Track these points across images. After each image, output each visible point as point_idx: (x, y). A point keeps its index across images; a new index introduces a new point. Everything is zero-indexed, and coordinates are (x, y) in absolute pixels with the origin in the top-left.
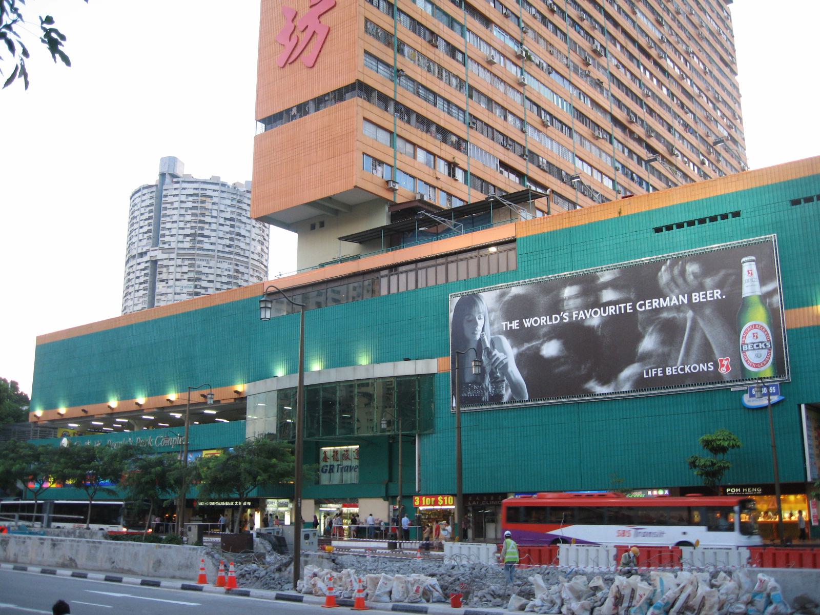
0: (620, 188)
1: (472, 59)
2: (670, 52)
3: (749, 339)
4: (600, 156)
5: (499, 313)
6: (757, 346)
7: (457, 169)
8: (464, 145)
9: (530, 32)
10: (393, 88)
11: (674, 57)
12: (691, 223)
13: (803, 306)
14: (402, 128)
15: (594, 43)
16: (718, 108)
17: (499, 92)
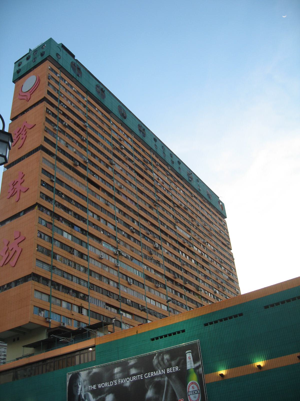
0: (171, 310)
1: (91, 258)
2: (195, 243)
3: (191, 389)
4: (160, 295)
5: (88, 382)
6: (194, 392)
7: (83, 309)
8: (87, 297)
9: (121, 243)
10: (50, 275)
11: (198, 246)
12: (166, 336)
13: (212, 372)
15: (155, 244)
16: (222, 266)
17: (105, 272)
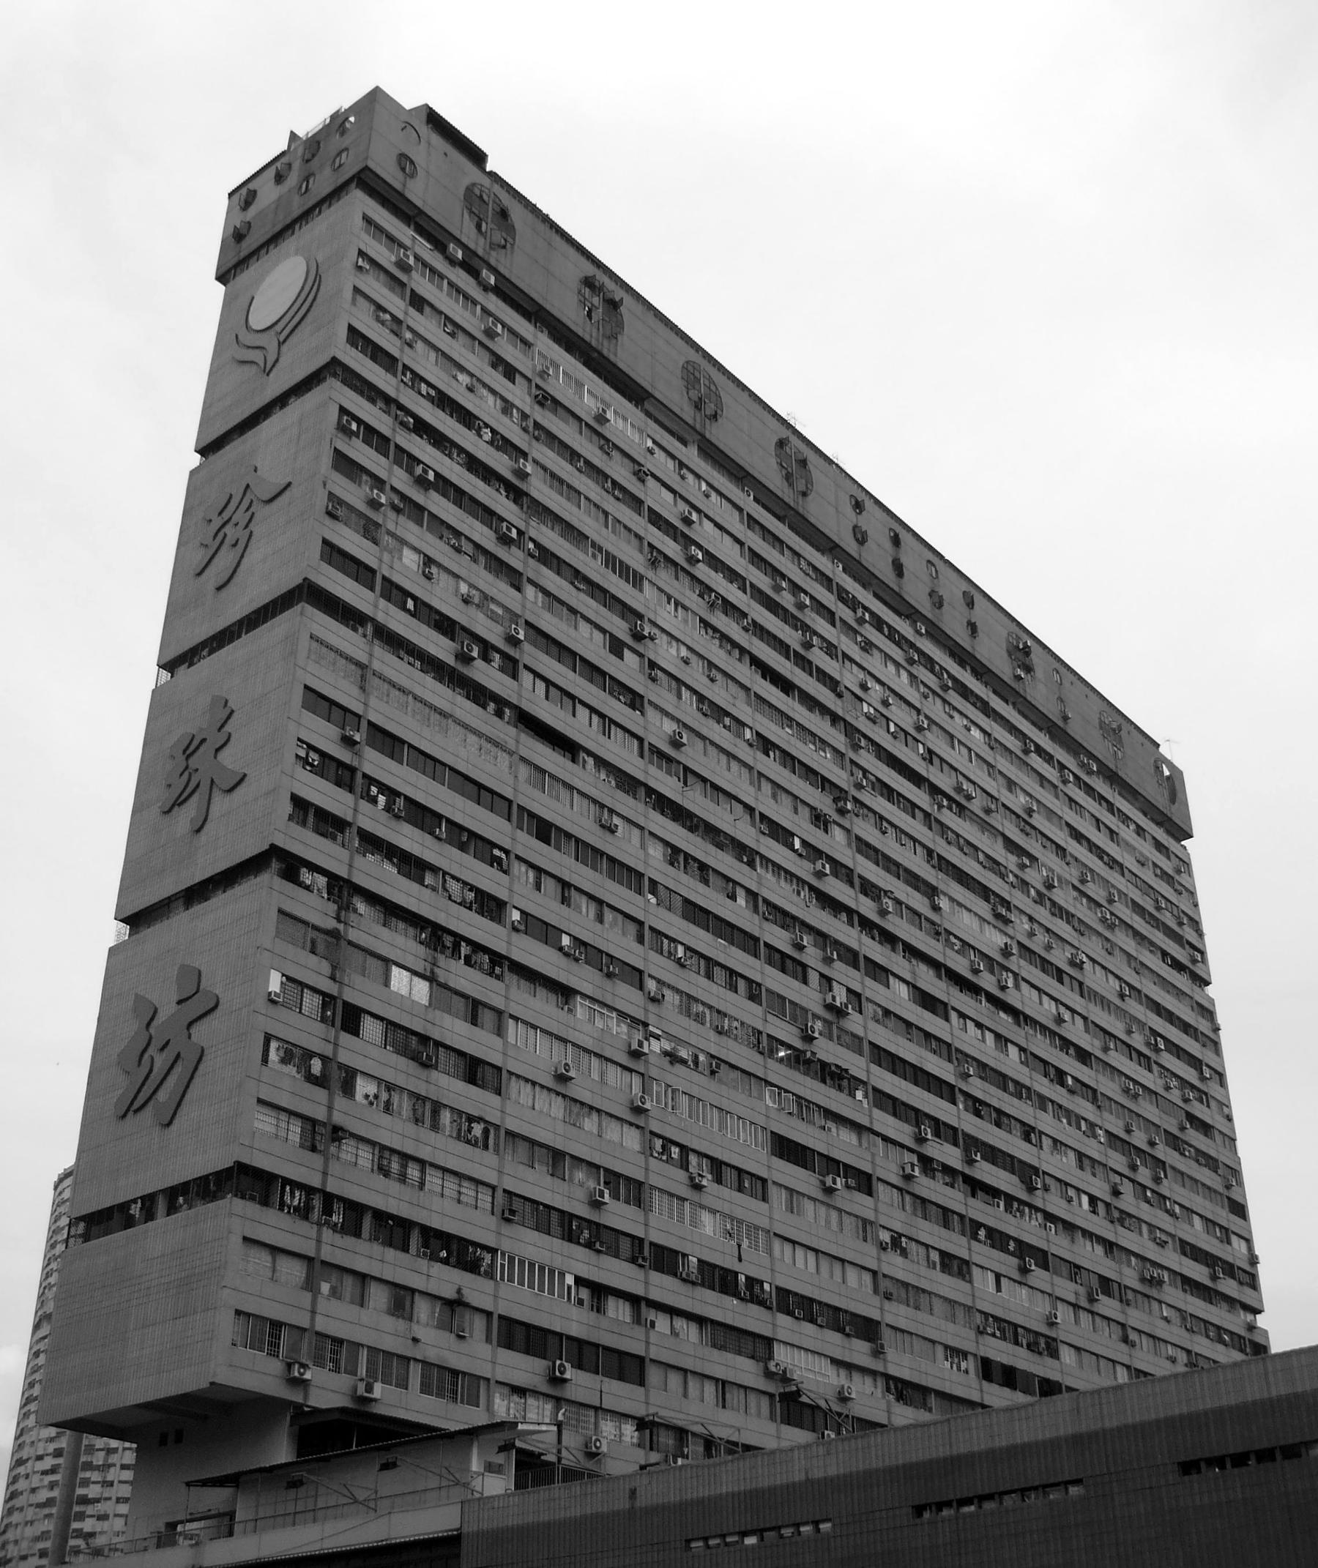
14: (338, 1248)
